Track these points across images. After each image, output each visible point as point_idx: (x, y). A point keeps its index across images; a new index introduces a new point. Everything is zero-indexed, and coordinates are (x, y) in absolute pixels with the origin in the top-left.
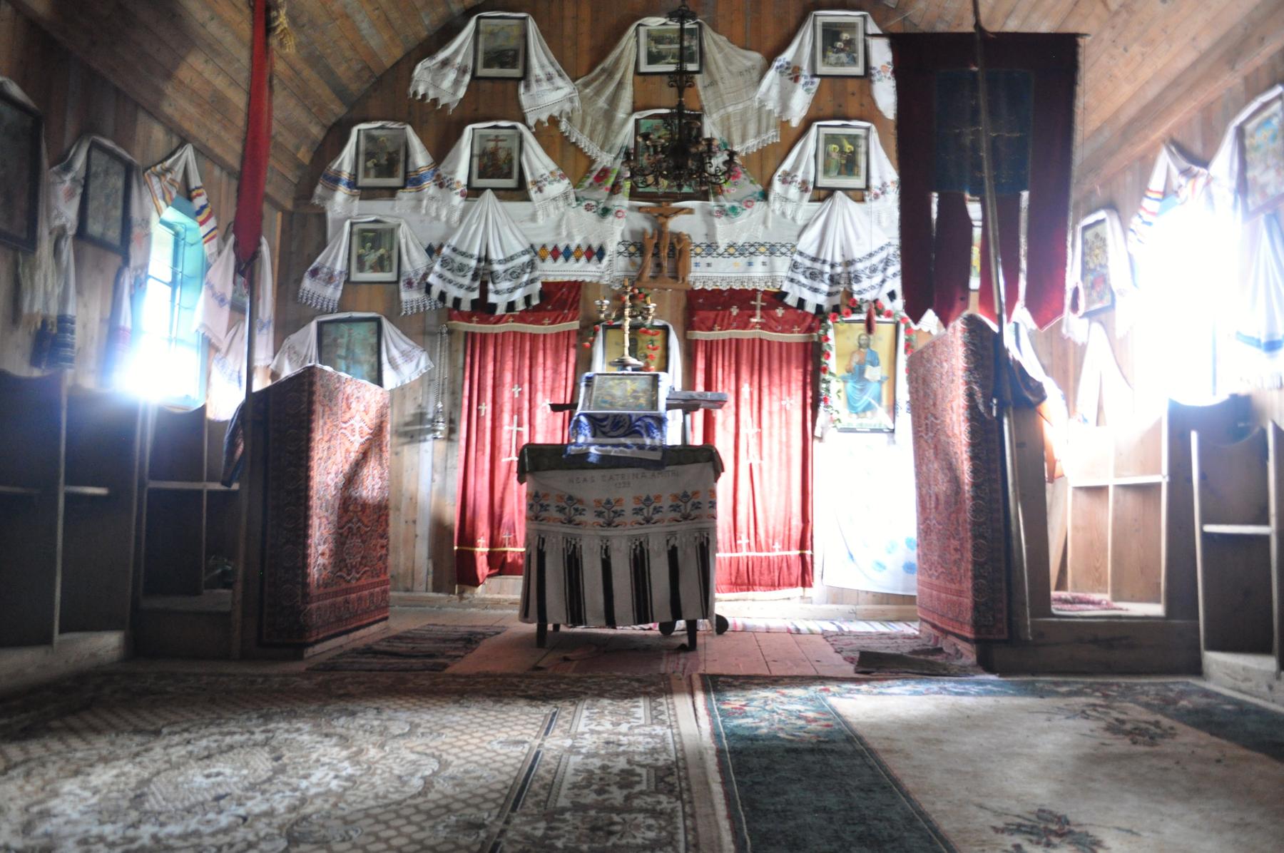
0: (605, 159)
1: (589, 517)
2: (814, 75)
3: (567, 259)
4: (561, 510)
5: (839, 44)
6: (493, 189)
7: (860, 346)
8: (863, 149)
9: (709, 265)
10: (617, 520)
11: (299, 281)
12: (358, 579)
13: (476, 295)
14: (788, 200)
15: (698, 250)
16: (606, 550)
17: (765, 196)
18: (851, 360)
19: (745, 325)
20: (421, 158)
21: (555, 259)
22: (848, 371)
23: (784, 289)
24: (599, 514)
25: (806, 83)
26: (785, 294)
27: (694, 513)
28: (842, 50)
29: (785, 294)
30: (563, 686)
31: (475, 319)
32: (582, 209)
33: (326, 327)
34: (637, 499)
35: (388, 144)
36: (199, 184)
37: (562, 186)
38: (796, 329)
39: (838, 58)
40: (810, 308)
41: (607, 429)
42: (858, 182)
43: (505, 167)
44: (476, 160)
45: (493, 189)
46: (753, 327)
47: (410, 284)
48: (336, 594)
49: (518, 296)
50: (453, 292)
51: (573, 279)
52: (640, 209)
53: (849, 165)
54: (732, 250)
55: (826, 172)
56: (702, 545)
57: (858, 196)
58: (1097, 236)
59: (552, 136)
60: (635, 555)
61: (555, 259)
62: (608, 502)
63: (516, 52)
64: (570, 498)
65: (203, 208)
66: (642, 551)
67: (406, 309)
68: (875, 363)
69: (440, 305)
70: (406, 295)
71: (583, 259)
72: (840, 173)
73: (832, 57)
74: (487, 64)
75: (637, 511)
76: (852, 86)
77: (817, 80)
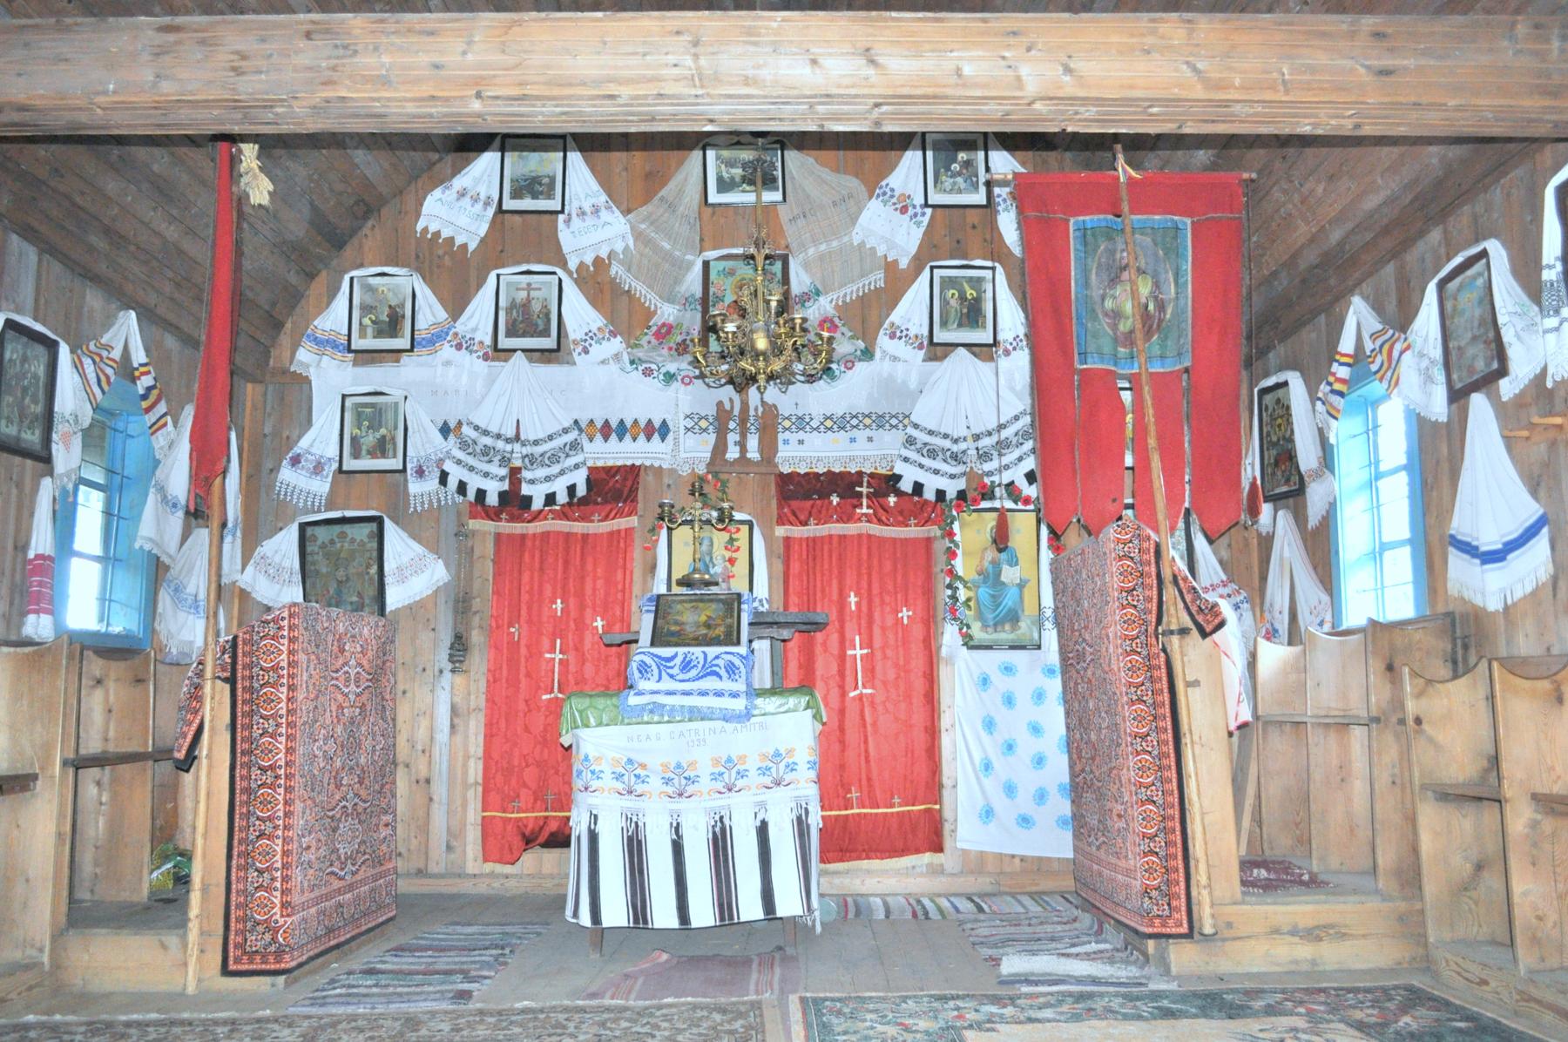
0: (667, 312)
1: (655, 783)
2: (926, 205)
4: (619, 777)
5: (955, 167)
8: (989, 295)
9: (801, 442)
10: (690, 789)
11: (275, 470)
12: (354, 874)
13: (505, 486)
14: (897, 358)
15: (787, 424)
17: (868, 354)
18: (982, 558)
19: (847, 517)
20: (430, 311)
21: (606, 438)
23: (897, 471)
25: (915, 215)
26: (898, 478)
28: (959, 174)
29: (898, 478)
30: (624, 1024)
31: (504, 516)
33: (309, 531)
34: (716, 762)
35: (390, 295)
36: (144, 360)
37: (617, 344)
38: (913, 521)
39: (955, 183)
40: (929, 495)
41: (675, 671)
42: (984, 336)
45: (524, 351)
46: (859, 520)
47: (420, 472)
48: (327, 897)
49: (559, 488)
50: (475, 483)
51: (629, 463)
53: (972, 314)
54: (829, 423)
55: (944, 324)
56: (799, 819)
57: (986, 351)
58: (1278, 401)
59: (597, 282)
61: (606, 438)
62: (679, 766)
63: (553, 179)
64: (630, 761)
65: (149, 389)
66: (723, 830)
67: (415, 505)
68: (1013, 562)
70: (415, 487)
71: (642, 437)
72: (960, 325)
73: (948, 182)
74: (516, 195)
75: (716, 777)
76: (973, 217)
77: (929, 211)
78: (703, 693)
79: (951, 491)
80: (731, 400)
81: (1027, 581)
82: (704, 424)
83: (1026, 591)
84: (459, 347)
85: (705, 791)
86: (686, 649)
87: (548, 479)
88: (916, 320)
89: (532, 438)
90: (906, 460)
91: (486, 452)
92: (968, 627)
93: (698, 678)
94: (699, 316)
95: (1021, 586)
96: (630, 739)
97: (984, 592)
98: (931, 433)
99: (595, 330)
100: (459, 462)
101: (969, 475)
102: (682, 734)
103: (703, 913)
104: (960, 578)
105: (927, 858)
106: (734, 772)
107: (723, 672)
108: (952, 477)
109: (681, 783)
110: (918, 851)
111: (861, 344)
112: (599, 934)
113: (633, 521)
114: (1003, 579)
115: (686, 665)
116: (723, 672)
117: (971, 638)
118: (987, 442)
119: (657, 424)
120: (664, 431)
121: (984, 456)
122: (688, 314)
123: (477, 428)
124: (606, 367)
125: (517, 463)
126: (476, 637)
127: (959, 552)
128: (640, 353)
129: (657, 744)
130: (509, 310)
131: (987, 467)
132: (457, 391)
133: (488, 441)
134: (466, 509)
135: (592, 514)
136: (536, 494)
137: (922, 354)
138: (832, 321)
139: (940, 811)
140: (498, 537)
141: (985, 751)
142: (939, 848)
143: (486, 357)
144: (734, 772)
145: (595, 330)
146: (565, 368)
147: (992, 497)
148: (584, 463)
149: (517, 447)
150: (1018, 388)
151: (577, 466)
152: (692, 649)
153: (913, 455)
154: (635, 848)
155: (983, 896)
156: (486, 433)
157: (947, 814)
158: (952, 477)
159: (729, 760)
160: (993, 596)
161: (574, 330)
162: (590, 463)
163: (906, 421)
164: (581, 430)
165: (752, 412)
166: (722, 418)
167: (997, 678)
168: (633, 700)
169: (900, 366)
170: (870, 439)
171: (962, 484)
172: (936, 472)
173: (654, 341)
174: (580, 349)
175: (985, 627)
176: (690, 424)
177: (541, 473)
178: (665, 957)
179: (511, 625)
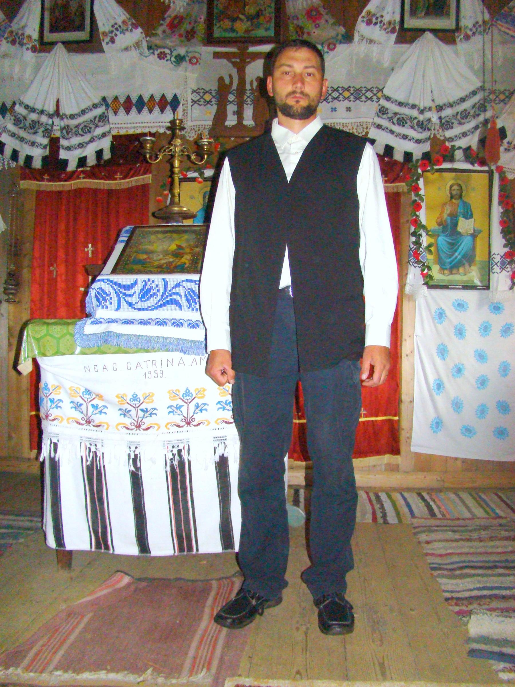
1: (112, 416)
3: (139, 111)
4: (77, 407)
6: (64, 43)
7: (452, 197)
10: (148, 421)
16: (135, 460)
17: (348, 38)
18: (442, 212)
21: (128, 111)
22: (440, 224)
24: (125, 413)
27: (199, 417)
31: (46, 177)
32: (153, 58)
34: (174, 394)
37: (138, 34)
41: (134, 300)
43: (77, 20)
44: (47, 14)
49: (90, 152)
52: (226, 56)
57: (447, 37)
60: (172, 466)
61: (128, 111)
62: (135, 397)
64: (88, 392)
66: (181, 463)
68: (468, 215)
69: (13, 164)
71: (157, 109)
72: (427, 14)
75: (174, 410)
78: (161, 323)
79: (418, 151)
80: (230, 76)
81: (480, 232)
82: (207, 97)
83: (478, 240)
84: (13, 42)
85: (163, 424)
86: (145, 277)
87: (81, 146)
88: (389, 9)
89: (68, 112)
90: (379, 127)
91: (34, 126)
92: (429, 268)
93: (157, 307)
94: (205, 10)
95: (474, 236)
96: (87, 369)
97: (442, 240)
98: (400, 104)
99: (120, 22)
100: (13, 135)
101: (434, 140)
102: (138, 365)
103: (162, 543)
104: (424, 227)
105: (387, 458)
106: (192, 406)
107: (183, 301)
108: (418, 141)
109: (138, 414)
110: (378, 452)
111: (342, 30)
112: (65, 557)
113: (148, 178)
114: (459, 229)
115: (146, 293)
116: (183, 301)
117: (431, 277)
118: (448, 112)
119: (169, 98)
120: (175, 103)
121: (446, 125)
122: (196, 7)
123: (27, 107)
124: (126, 53)
125: (58, 134)
126: (26, 274)
127: (423, 205)
128: (156, 41)
129: (115, 376)
130: (52, 10)
131: (449, 134)
132: (12, 78)
133: (34, 116)
134: (19, 172)
135: (115, 173)
136: (70, 158)
137: (394, 36)
138: (317, 10)
139: (399, 421)
140: (39, 193)
141: (437, 372)
142: (396, 451)
143: (34, 49)
144: (192, 406)
145: (120, 22)
146: (95, 56)
147: (452, 159)
148: (109, 132)
149: (57, 121)
150: (476, 68)
151: (104, 135)
152: (152, 277)
153: (385, 123)
154: (94, 477)
155: (431, 491)
156: (33, 110)
157: (404, 424)
158: (418, 141)
159: (187, 393)
160: (449, 243)
161: (103, 25)
162: (114, 132)
163: (379, 94)
164: (107, 106)
165: (248, 87)
166: (222, 90)
167: (451, 313)
168: (89, 328)
169: (375, 49)
170: (349, 109)
171: (426, 147)
172: (405, 137)
173: (168, 31)
174: (107, 39)
175: (442, 269)
176: (196, 97)
177: (76, 140)
178: (126, 580)
179: (52, 265)
